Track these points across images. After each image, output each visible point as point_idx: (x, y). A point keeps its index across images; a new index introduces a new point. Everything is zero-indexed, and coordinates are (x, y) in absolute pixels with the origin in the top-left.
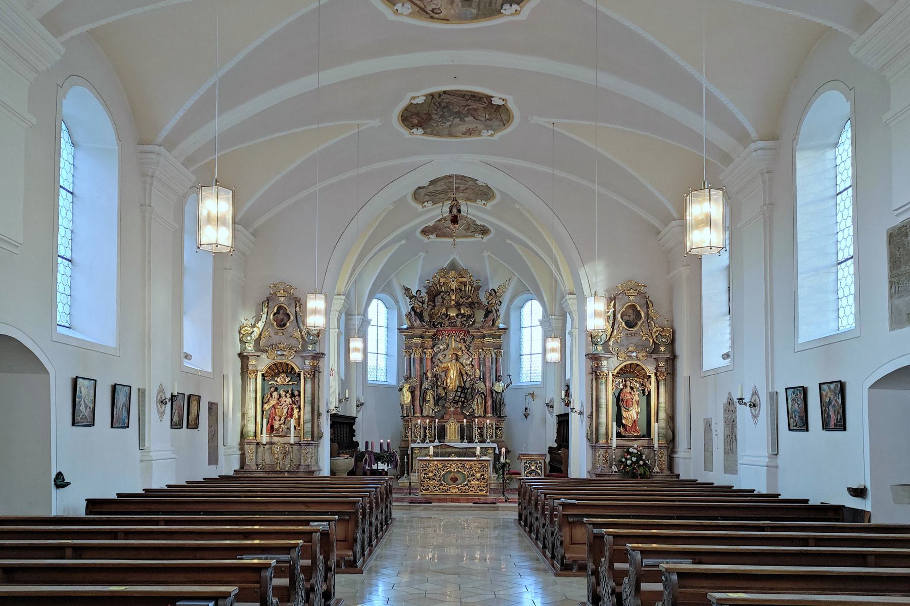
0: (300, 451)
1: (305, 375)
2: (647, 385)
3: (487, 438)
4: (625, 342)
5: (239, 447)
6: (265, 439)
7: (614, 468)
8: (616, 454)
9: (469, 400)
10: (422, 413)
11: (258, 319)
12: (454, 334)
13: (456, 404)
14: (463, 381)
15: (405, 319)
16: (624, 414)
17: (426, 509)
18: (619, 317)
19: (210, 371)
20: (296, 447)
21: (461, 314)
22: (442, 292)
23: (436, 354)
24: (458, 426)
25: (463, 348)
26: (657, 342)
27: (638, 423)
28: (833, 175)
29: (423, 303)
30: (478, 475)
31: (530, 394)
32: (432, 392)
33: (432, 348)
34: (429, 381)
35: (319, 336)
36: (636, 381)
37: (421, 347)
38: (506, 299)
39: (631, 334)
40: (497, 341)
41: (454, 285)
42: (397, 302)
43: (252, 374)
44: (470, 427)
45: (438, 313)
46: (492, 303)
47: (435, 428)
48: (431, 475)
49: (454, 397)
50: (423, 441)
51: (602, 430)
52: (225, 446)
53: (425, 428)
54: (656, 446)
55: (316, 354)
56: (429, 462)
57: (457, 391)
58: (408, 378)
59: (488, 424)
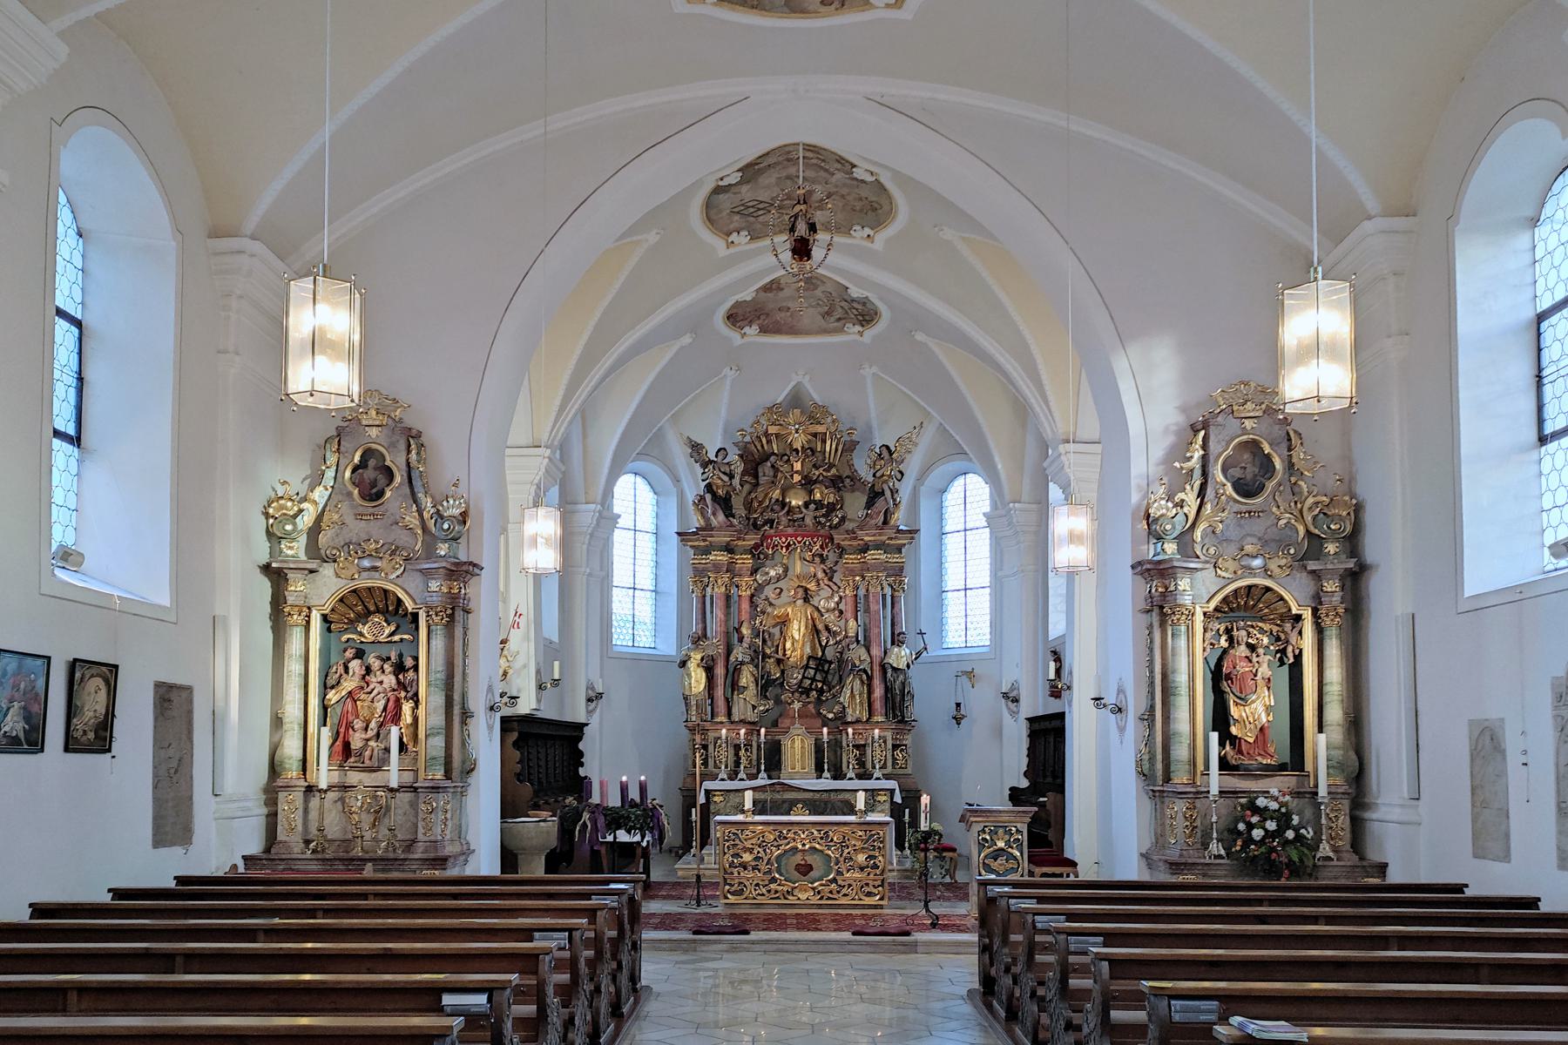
0: (414, 805)
1: (428, 616)
2: (1293, 638)
3: (874, 767)
4: (1234, 533)
5: (264, 797)
6: (324, 776)
7: (1215, 848)
8: (1217, 814)
9: (834, 687)
10: (729, 714)
11: (316, 480)
12: (799, 542)
13: (804, 697)
14: (821, 645)
15: (693, 512)
16: (1234, 711)
17: (734, 949)
18: (1217, 474)
19: (165, 601)
20: (406, 797)
21: (815, 502)
22: (773, 454)
23: (760, 588)
25: (820, 575)
26: (1317, 532)
27: (1270, 734)
28: (1529, 279)
29: (731, 477)
30: (861, 858)
32: (751, 668)
33: (752, 574)
34: (745, 645)
35: (465, 523)
36: (1262, 631)
37: (727, 571)
38: (912, 466)
39: (1250, 512)
40: (894, 558)
41: (799, 441)
42: (677, 480)
43: (295, 617)
44: (836, 745)
46: (883, 475)
48: (747, 857)
50: (733, 776)
51: (1181, 752)
52: (216, 795)
53: (737, 748)
54: (1323, 791)
55: (456, 564)
56: (742, 827)
57: (807, 667)
58: (699, 639)
59: (876, 737)
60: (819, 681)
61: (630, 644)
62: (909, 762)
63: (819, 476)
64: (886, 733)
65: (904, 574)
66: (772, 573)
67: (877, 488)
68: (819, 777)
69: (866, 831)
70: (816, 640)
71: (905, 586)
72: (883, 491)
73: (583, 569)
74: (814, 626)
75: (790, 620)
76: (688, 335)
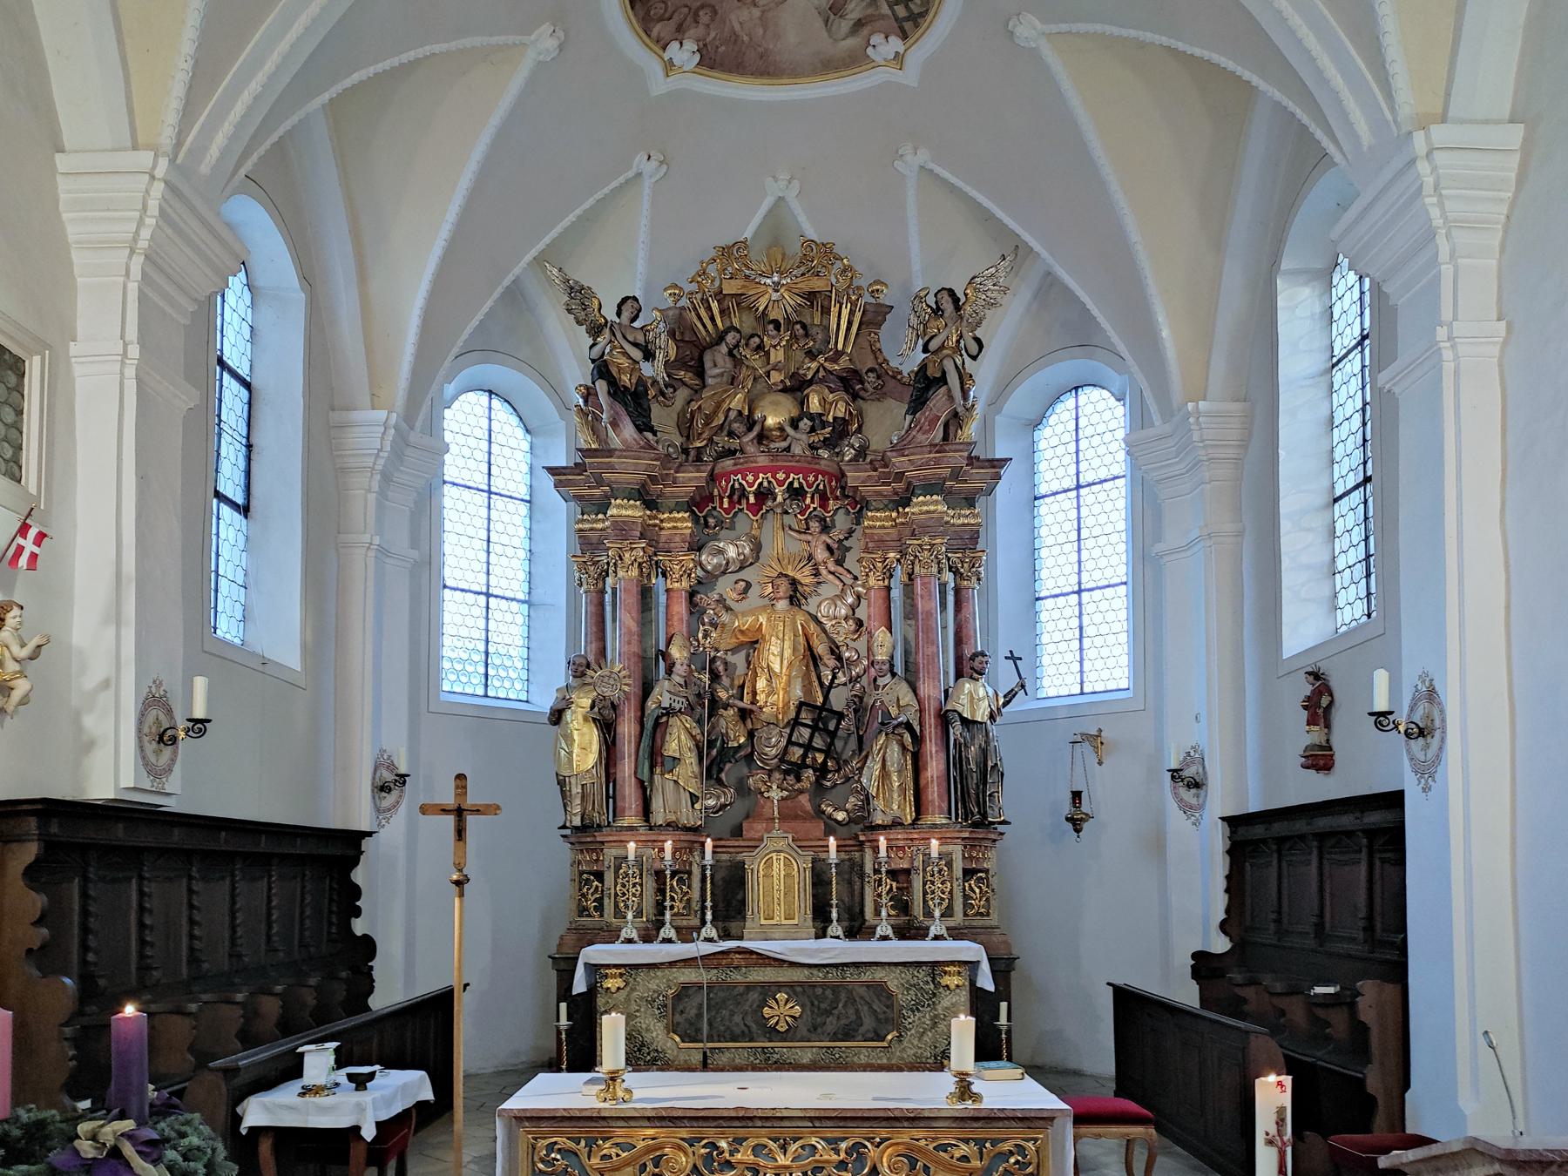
3: (929, 914)
9: (846, 762)
14: (821, 684)
21: (811, 417)
23: (707, 581)
24: (802, 865)
25: (821, 554)
31: (1087, 737)
32: (689, 722)
34: (677, 678)
40: (961, 518)
44: (853, 871)
45: (715, 412)
46: (942, 347)
47: (704, 868)
49: (786, 747)
53: (659, 875)
57: (795, 723)
59: (935, 854)
60: (819, 750)
61: (480, 691)
62: (992, 902)
63: (818, 371)
64: (950, 848)
65: (979, 547)
66: (732, 552)
67: (933, 372)
68: (821, 934)
69: (980, 1143)
70: (813, 674)
71: (981, 569)
72: (944, 373)
73: (366, 538)
74: (810, 648)
75: (763, 637)
76: (546, 28)
